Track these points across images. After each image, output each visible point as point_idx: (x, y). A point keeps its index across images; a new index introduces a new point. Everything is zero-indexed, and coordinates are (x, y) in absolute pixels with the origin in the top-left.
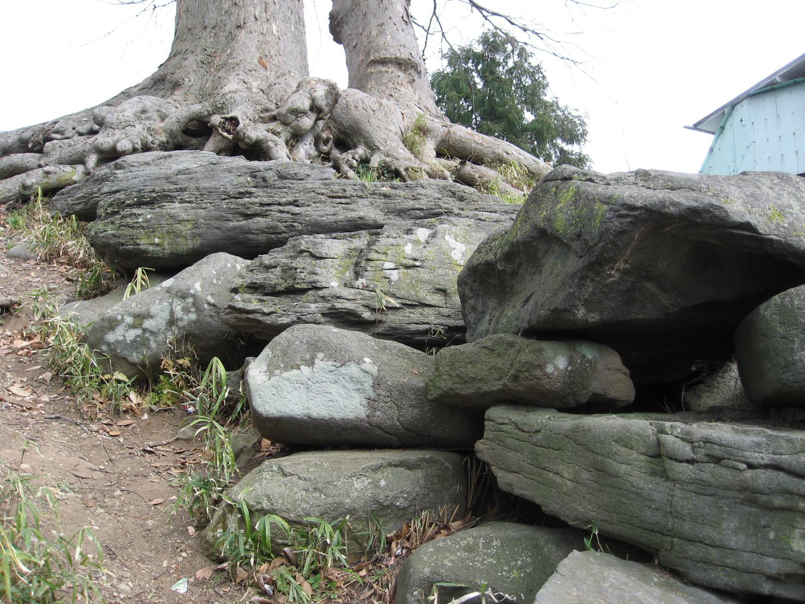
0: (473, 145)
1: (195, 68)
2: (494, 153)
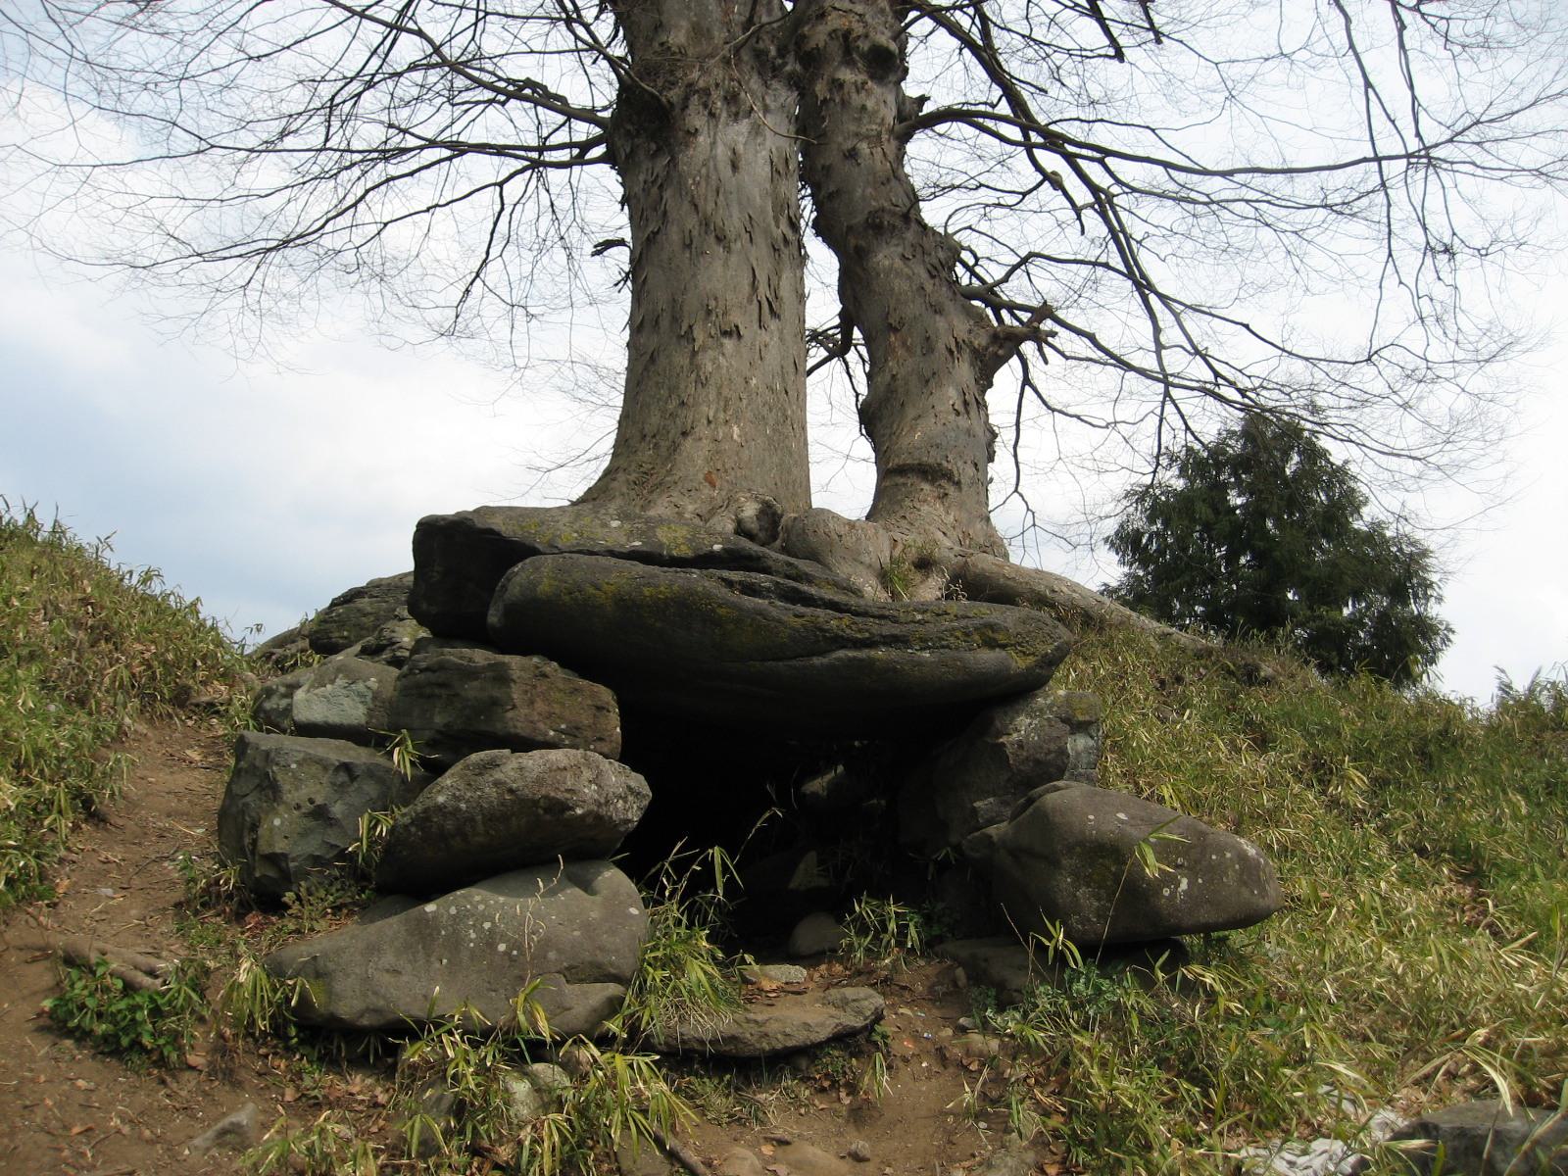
1: (625, 490)
2: (1033, 591)
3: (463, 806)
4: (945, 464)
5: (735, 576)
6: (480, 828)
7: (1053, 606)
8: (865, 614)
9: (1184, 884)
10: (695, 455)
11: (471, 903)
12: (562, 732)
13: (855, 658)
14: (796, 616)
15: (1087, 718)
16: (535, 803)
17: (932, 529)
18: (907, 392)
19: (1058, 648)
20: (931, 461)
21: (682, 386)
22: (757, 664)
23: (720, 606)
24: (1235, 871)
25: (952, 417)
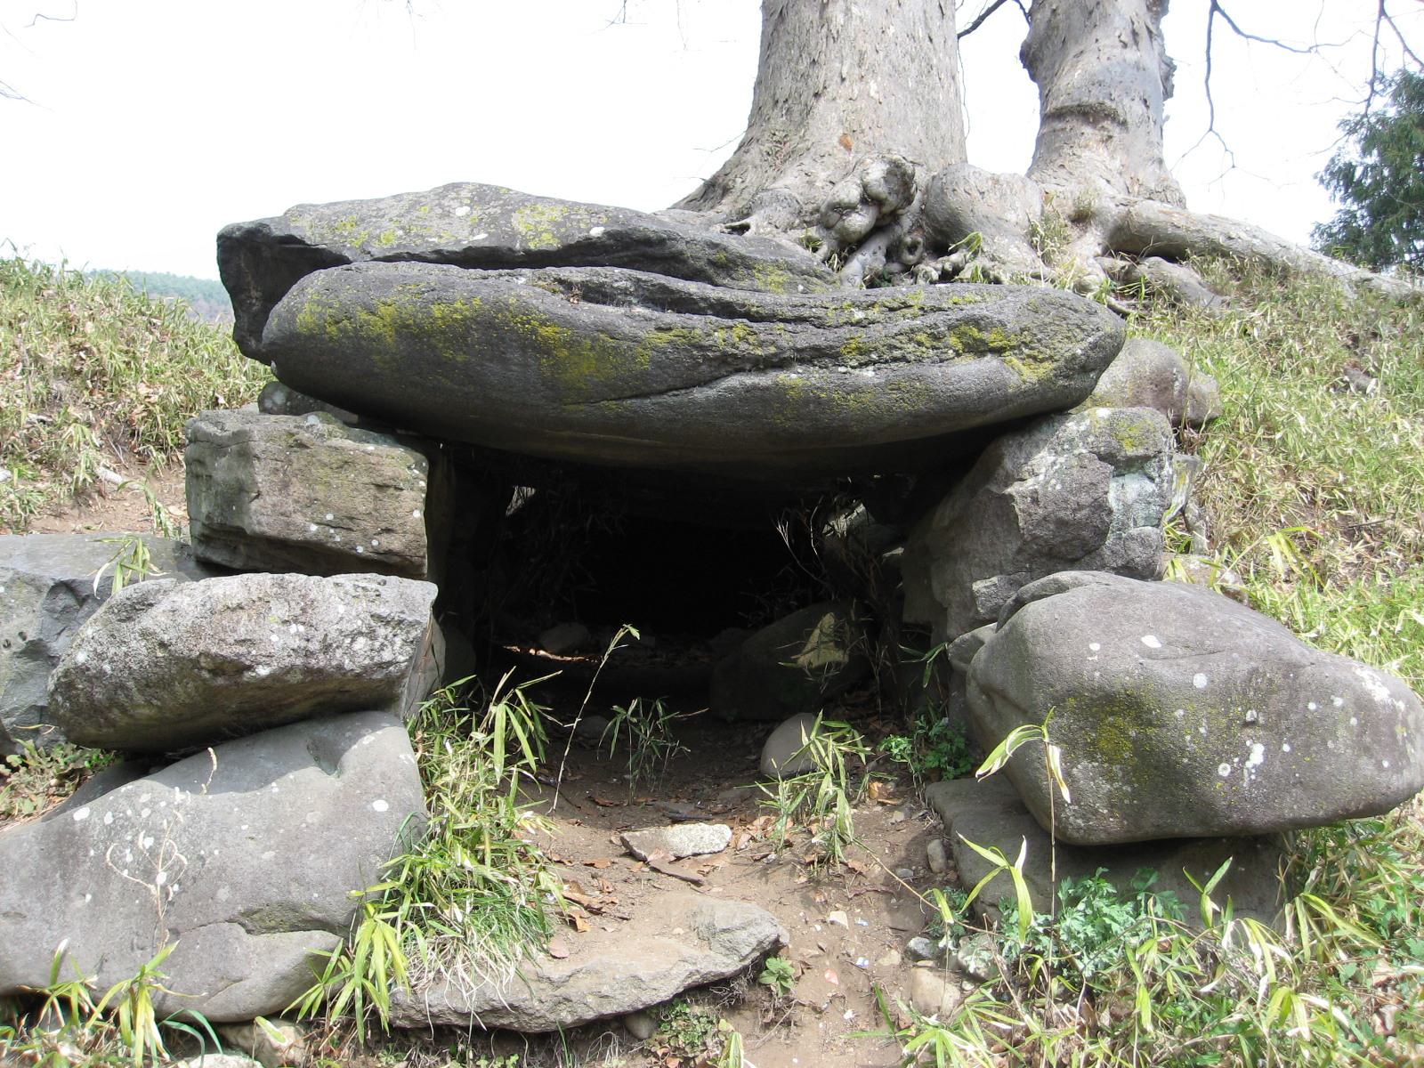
0: (1170, 230)
3: (107, 667)
4: (1108, 103)
5: (575, 274)
6: (139, 698)
7: (1225, 255)
8: (771, 318)
9: (1257, 755)
10: (827, 121)
11: (133, 806)
12: (328, 524)
13: (755, 387)
14: (659, 329)
15: (1141, 452)
16: (195, 663)
17: (1093, 176)
18: (1069, 28)
19: (1094, 346)
20: (1092, 100)
21: (813, 43)
22: (612, 404)
23: (543, 323)
24: (1349, 728)
25: (1118, 51)
